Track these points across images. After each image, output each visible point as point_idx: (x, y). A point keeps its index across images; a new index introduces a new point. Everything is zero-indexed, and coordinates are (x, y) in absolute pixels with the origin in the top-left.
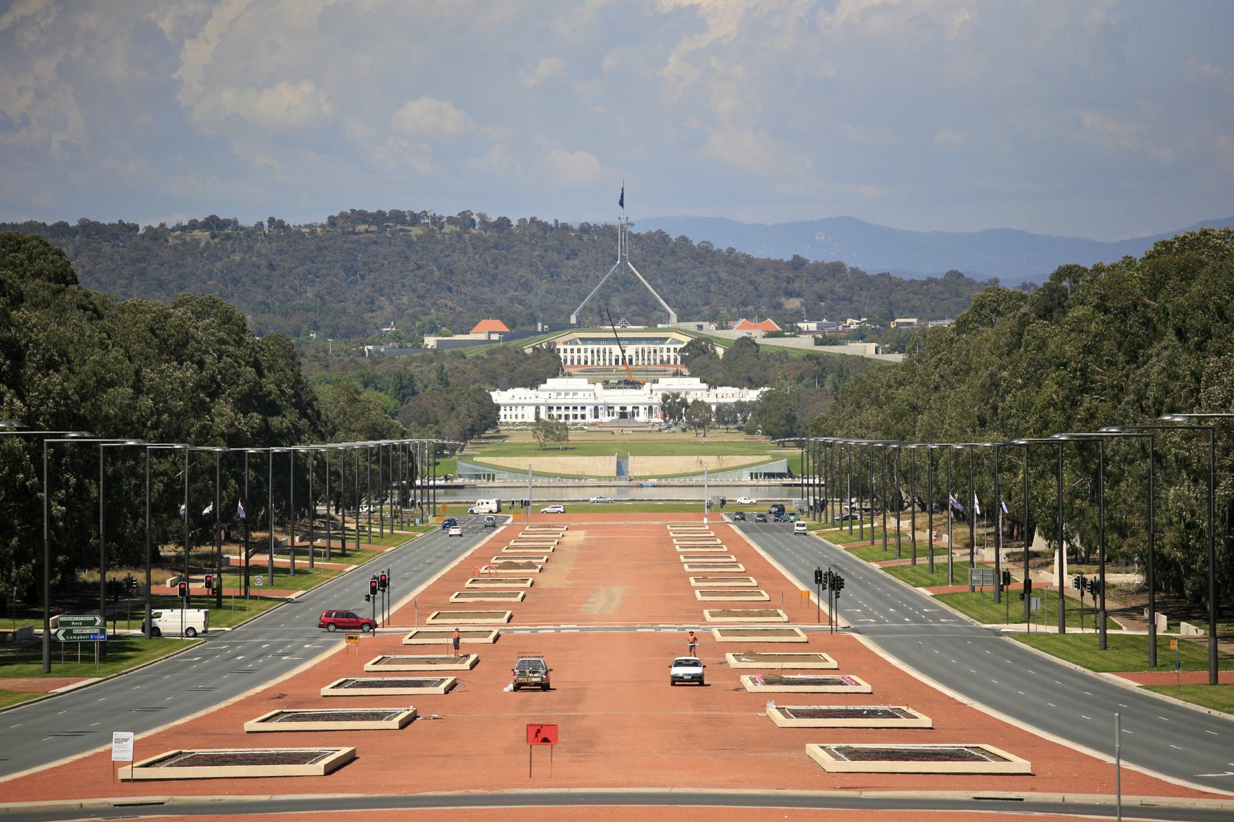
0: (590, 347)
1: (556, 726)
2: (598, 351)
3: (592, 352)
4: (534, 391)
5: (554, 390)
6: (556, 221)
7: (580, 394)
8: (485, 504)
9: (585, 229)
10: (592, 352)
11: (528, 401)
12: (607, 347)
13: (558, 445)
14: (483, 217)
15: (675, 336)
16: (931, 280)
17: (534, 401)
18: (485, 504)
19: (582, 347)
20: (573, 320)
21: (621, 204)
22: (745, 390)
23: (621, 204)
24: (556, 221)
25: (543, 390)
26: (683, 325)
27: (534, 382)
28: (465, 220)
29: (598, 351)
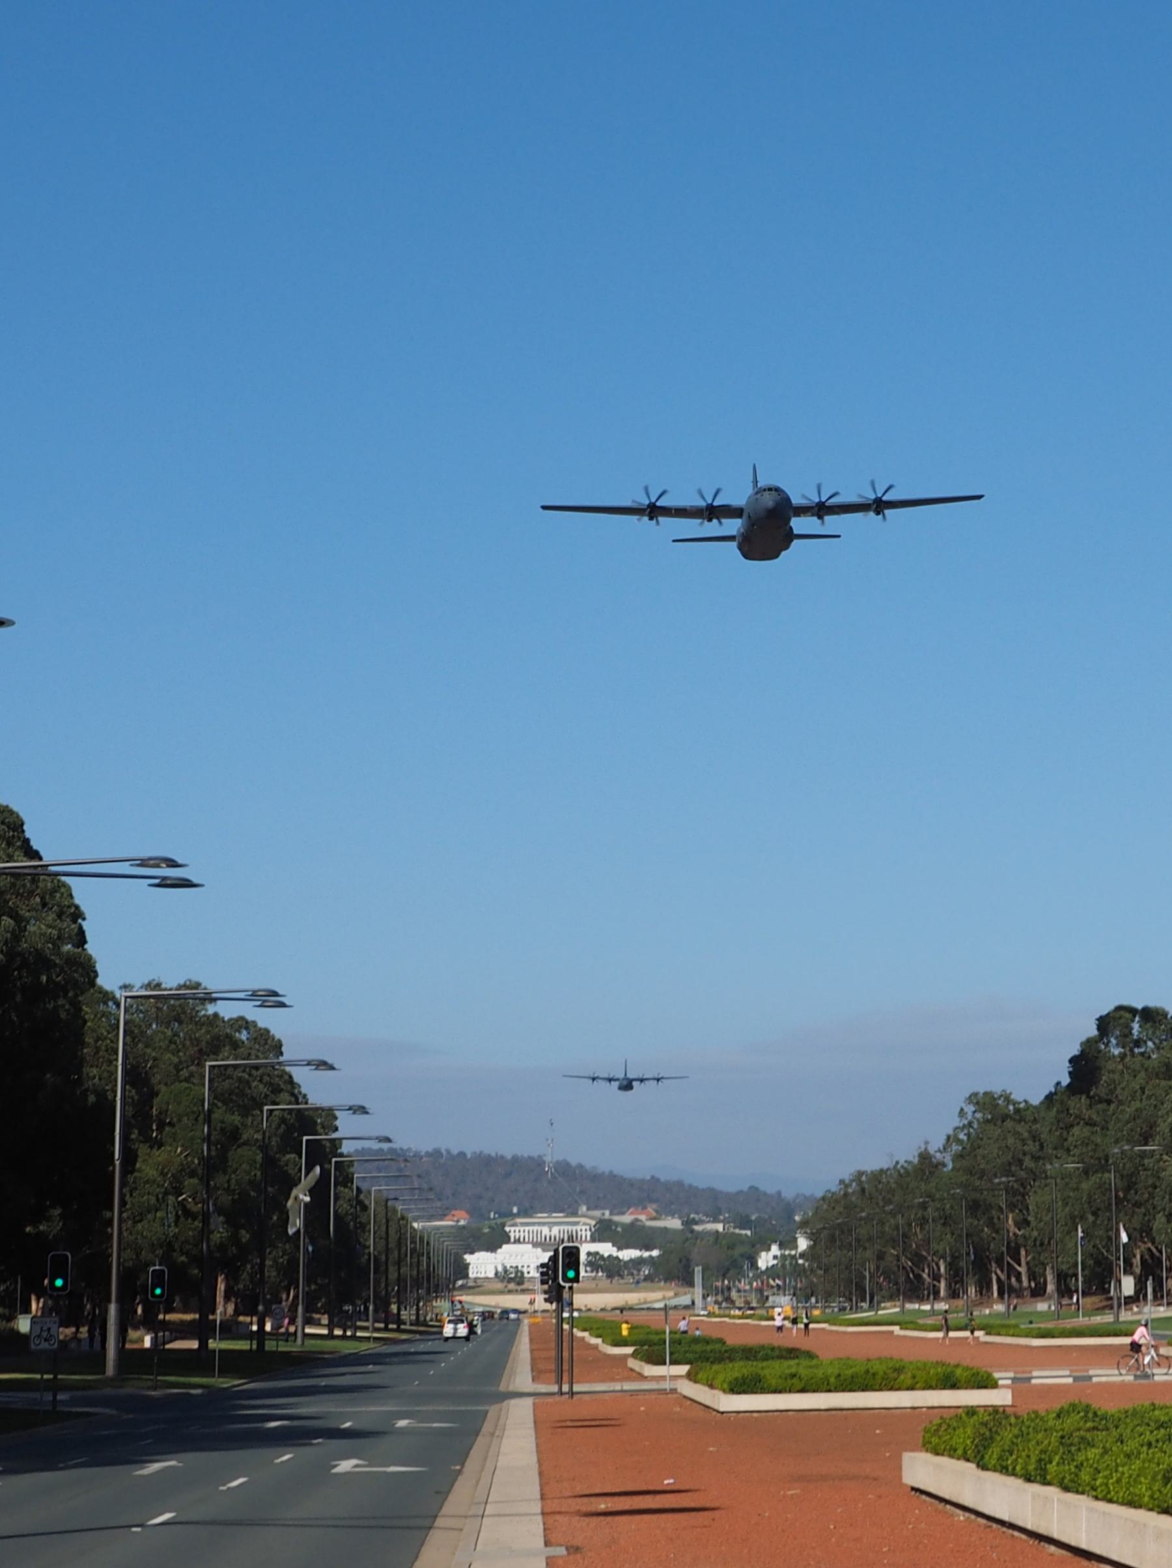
0: (527, 1229)
1: (547, 1558)
2: (533, 1232)
3: (529, 1232)
4: (493, 1254)
5: (508, 1253)
6: (497, 1154)
7: (526, 1256)
8: (529, 1269)
9: (515, 1159)
10: (529, 1232)
11: (489, 1261)
12: (539, 1228)
13: (519, 1288)
14: (448, 1152)
15: (583, 1220)
16: (740, 1192)
17: (493, 1260)
18: (529, 1269)
19: (522, 1229)
20: (515, 1210)
21: (437, 1492)
22: (643, 1251)
23: (437, 1492)
24: (497, 1154)
25: (501, 1253)
26: (591, 1213)
27: (493, 1247)
28: (437, 1153)
29: (533, 1232)
